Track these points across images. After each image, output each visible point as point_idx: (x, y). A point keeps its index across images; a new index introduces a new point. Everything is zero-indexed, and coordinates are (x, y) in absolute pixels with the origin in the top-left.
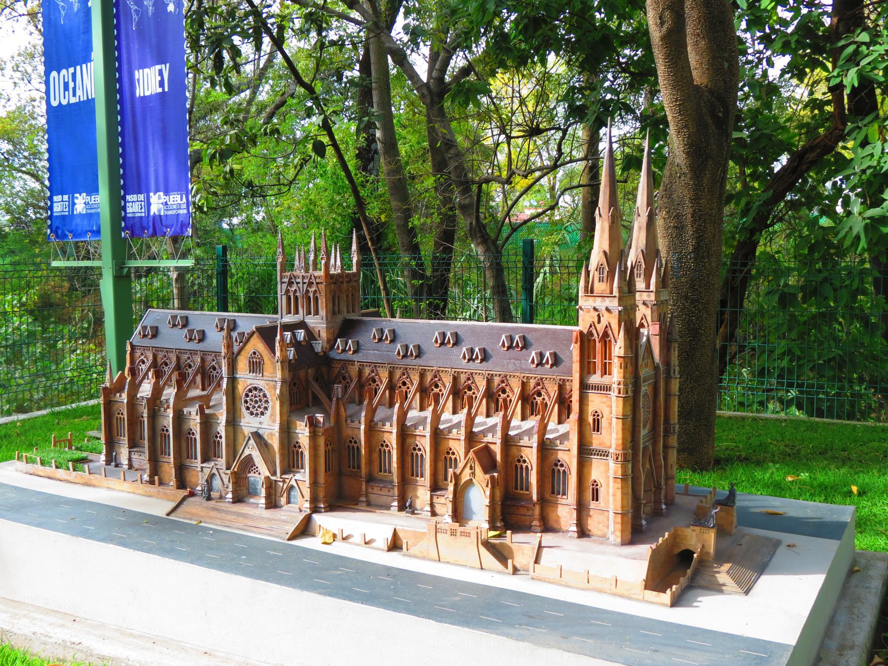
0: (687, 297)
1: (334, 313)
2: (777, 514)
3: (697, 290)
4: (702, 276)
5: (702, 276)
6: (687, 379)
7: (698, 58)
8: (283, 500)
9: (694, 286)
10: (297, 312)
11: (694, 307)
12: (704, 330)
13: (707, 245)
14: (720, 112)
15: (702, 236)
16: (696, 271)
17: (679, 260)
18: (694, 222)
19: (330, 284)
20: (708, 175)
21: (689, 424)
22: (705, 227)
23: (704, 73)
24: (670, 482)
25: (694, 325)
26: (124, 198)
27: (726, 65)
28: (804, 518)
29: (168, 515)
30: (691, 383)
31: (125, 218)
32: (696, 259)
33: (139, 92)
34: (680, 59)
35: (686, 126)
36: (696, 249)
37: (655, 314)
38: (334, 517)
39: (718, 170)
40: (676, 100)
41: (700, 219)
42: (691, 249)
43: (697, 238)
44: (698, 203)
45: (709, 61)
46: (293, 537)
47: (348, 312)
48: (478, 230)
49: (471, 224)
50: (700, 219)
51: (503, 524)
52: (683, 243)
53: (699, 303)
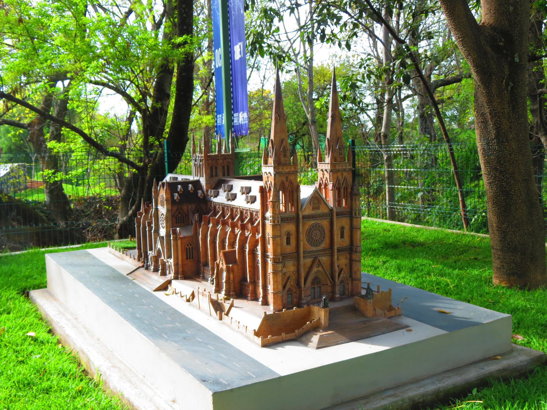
0: (496, 169)
1: (212, 176)
2: (444, 313)
3: (503, 164)
4: (505, 155)
5: (505, 155)
6: (509, 225)
7: (488, 6)
8: (168, 272)
9: (500, 161)
10: (216, 175)
11: (503, 176)
12: (514, 192)
13: (504, 133)
14: (501, 41)
15: (500, 127)
16: (500, 151)
17: (488, 144)
18: (492, 118)
19: (208, 160)
20: (494, 86)
21: (515, 257)
22: (500, 121)
23: (491, 16)
24: (354, 282)
25: (505, 188)
26: (233, 115)
27: (511, 8)
28: (458, 317)
29: (127, 275)
30: (512, 228)
31: (233, 126)
32: (498, 143)
33: (236, 59)
34: (455, 10)
35: (469, 55)
36: (497, 136)
37: (331, 177)
38: (182, 283)
39: (502, 82)
40: (459, 38)
41: (496, 116)
42: (493, 136)
43: (497, 129)
44: (492, 105)
45: (495, 7)
46: (159, 289)
47: (224, 175)
48: (541, 126)
49: (537, 122)
50: (496, 116)
51: (234, 293)
52: (488, 133)
53: (506, 173)
